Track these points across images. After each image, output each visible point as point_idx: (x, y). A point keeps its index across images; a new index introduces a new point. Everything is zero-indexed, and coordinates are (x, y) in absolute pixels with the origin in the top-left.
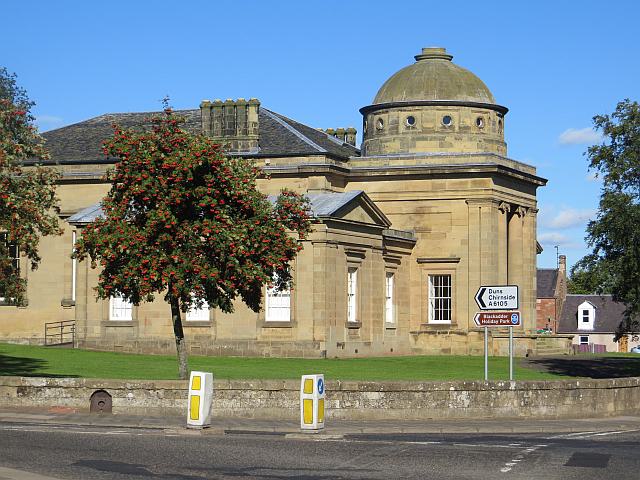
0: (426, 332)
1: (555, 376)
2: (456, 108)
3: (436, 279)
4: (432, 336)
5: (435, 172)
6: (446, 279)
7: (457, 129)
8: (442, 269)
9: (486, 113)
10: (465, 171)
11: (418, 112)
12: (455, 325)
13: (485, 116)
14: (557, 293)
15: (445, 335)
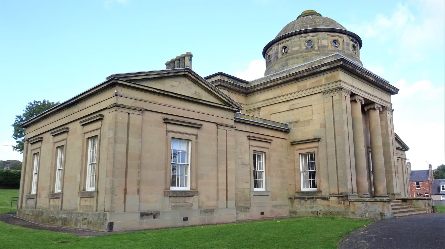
0: (298, 198)
1: (225, 221)
2: (315, 34)
3: (304, 155)
4: (303, 201)
5: (298, 76)
6: (312, 156)
7: (317, 48)
8: (308, 148)
9: (341, 37)
10: (318, 70)
11: (289, 42)
12: (319, 191)
13: (340, 40)
14: (429, 179)
15: (312, 200)
